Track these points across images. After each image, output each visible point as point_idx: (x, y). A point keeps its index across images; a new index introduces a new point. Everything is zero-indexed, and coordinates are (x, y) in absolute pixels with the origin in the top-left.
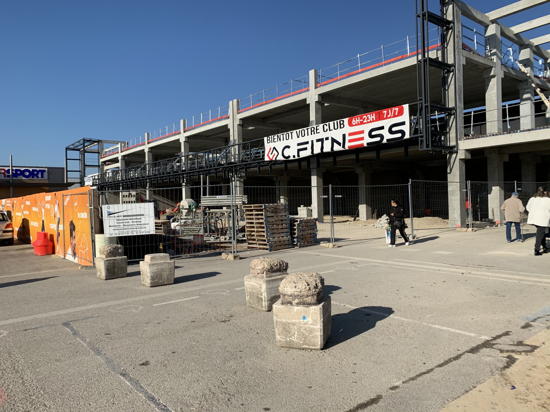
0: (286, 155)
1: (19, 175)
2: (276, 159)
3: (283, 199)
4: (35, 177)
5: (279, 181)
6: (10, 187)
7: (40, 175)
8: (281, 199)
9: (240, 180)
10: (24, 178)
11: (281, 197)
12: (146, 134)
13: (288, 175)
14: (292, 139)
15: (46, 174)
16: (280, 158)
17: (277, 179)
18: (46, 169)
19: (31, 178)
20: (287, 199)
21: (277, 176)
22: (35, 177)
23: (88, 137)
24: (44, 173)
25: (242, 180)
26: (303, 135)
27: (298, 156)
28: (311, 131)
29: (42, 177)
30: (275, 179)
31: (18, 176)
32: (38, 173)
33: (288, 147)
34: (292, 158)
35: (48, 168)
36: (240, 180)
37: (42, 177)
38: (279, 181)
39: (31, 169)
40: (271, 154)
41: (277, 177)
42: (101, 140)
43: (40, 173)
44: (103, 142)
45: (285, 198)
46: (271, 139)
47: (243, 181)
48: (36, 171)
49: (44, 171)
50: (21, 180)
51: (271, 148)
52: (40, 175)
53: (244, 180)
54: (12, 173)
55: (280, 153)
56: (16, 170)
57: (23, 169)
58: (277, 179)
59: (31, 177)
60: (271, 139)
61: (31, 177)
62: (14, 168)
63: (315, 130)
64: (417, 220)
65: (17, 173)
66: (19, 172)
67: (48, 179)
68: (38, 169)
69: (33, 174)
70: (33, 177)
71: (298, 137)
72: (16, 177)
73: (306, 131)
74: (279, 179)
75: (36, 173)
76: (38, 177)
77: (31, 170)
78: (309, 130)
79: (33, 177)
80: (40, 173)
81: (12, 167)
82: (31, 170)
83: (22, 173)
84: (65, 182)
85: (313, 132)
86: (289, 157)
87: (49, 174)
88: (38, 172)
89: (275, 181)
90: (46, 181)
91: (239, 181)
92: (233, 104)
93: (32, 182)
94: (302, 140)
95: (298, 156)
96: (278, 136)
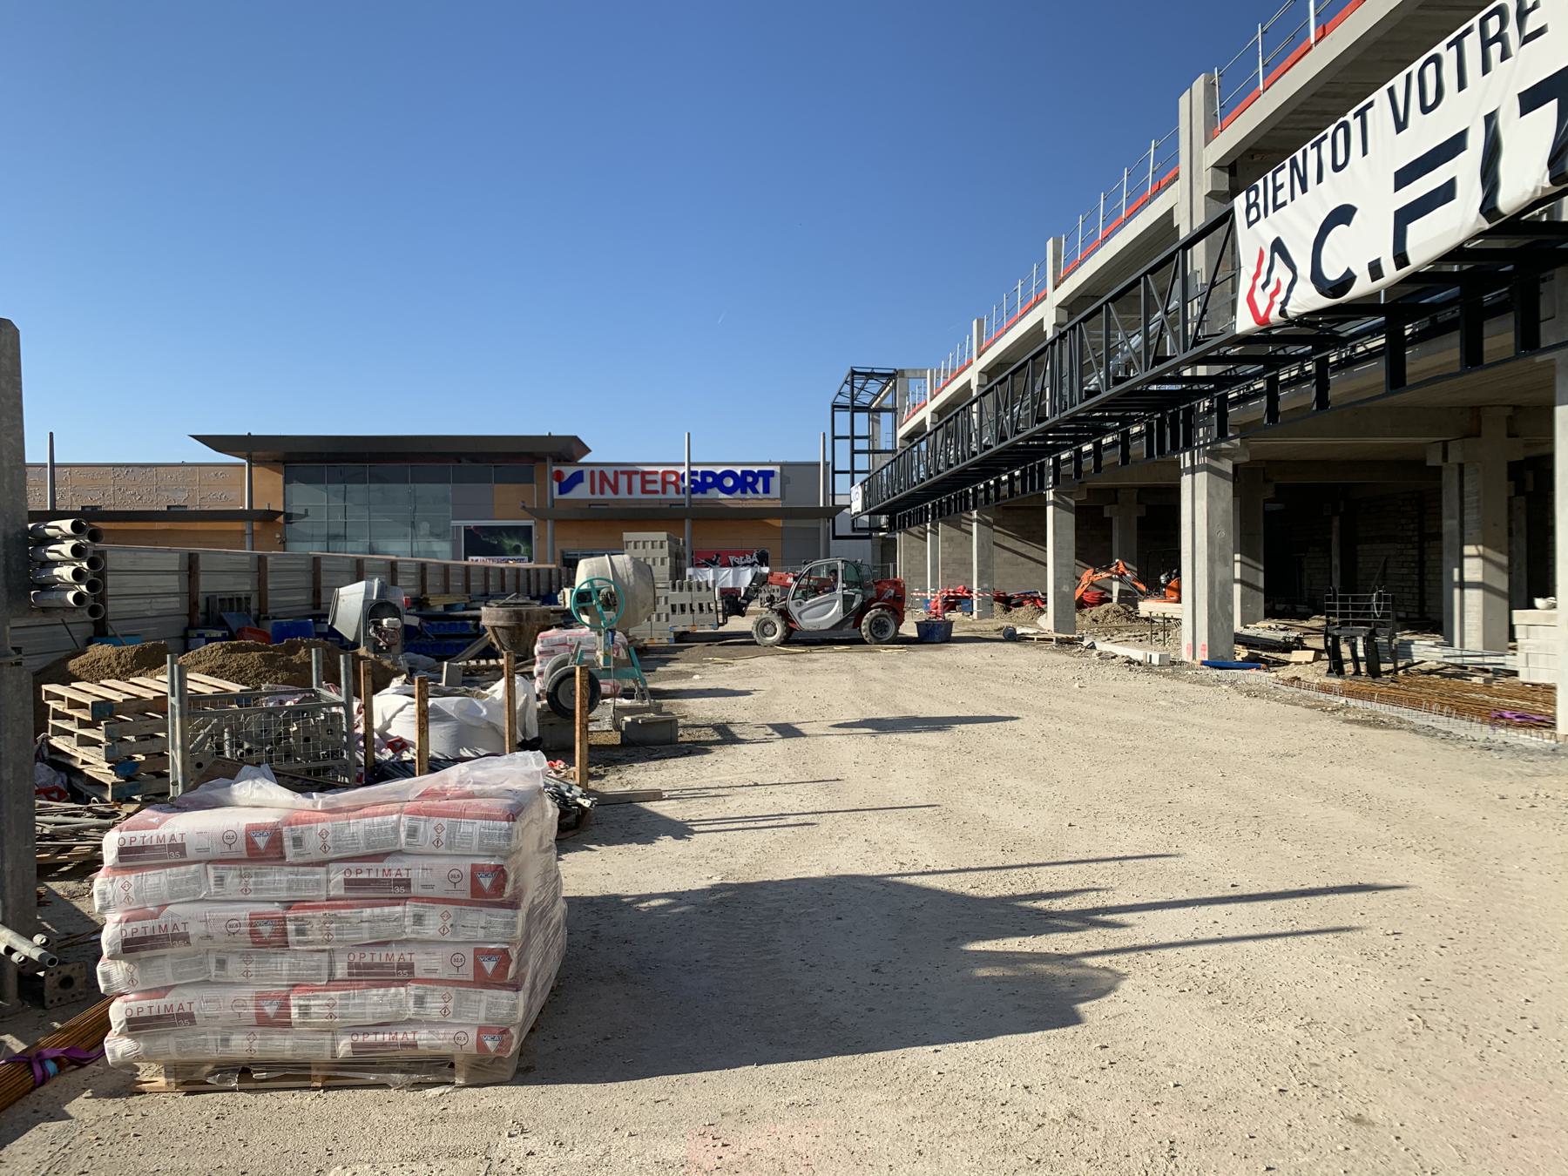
0: (1332, 273)
1: (711, 486)
2: (1282, 313)
3: (1478, 562)
4: (749, 490)
5: (1461, 466)
6: (683, 520)
7: (760, 486)
8: (1467, 562)
9: (1215, 464)
10: (722, 496)
11: (1469, 550)
12: (975, 322)
13: (1511, 435)
14: (1365, 153)
15: (775, 483)
16: (1307, 299)
17: (1445, 457)
18: (777, 469)
19: (738, 494)
20: (1504, 560)
21: (1445, 443)
22: (749, 490)
23: (865, 364)
24: (771, 479)
25: (1227, 466)
26: (1430, 100)
27: (1401, 259)
28: (1486, 44)
29: (767, 490)
30: (1434, 460)
31: (709, 491)
32: (756, 481)
33: (1343, 215)
34: (1363, 286)
35: (782, 465)
36: (1215, 464)
37: (767, 490)
38: (1461, 466)
39: (738, 470)
40: (1264, 286)
41: (1445, 443)
42: (903, 371)
43: (761, 479)
44: (907, 374)
45: (1491, 554)
46: (1261, 201)
47: (1230, 471)
48: (711, 474)
49: (772, 473)
50: (716, 501)
51: (1261, 253)
52: (760, 486)
53: (1235, 467)
54: (692, 482)
55: (1305, 269)
56: (704, 474)
57: (719, 470)
58: (1445, 457)
59: (739, 491)
60: (1261, 201)
61: (739, 491)
62: (699, 469)
63: (1512, 30)
64: (1178, 215)
65: (705, 482)
66: (710, 480)
67: (783, 497)
68: (756, 469)
69: (744, 482)
70: (744, 491)
71: (1401, 126)
72: (704, 492)
73: (1449, 58)
74: (1455, 456)
75: (750, 479)
76: (755, 491)
77: (739, 473)
78: (1472, 44)
79: (744, 491)
80: (761, 479)
81: (690, 464)
82: (739, 473)
83: (718, 480)
84: (821, 505)
85: (1496, 49)
86: (1348, 280)
87: (784, 480)
88: (756, 476)
89: (1439, 469)
90: (777, 501)
91: (1209, 469)
92: (1192, 103)
93: (740, 506)
94: (1426, 133)
95: (1401, 259)
96: (1294, 164)
